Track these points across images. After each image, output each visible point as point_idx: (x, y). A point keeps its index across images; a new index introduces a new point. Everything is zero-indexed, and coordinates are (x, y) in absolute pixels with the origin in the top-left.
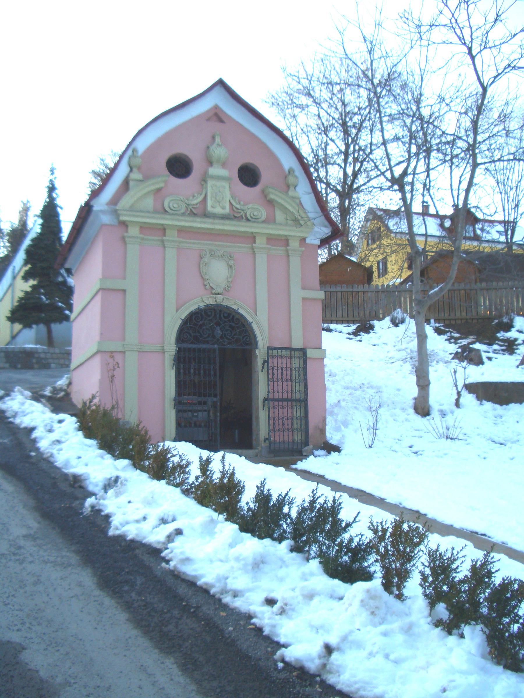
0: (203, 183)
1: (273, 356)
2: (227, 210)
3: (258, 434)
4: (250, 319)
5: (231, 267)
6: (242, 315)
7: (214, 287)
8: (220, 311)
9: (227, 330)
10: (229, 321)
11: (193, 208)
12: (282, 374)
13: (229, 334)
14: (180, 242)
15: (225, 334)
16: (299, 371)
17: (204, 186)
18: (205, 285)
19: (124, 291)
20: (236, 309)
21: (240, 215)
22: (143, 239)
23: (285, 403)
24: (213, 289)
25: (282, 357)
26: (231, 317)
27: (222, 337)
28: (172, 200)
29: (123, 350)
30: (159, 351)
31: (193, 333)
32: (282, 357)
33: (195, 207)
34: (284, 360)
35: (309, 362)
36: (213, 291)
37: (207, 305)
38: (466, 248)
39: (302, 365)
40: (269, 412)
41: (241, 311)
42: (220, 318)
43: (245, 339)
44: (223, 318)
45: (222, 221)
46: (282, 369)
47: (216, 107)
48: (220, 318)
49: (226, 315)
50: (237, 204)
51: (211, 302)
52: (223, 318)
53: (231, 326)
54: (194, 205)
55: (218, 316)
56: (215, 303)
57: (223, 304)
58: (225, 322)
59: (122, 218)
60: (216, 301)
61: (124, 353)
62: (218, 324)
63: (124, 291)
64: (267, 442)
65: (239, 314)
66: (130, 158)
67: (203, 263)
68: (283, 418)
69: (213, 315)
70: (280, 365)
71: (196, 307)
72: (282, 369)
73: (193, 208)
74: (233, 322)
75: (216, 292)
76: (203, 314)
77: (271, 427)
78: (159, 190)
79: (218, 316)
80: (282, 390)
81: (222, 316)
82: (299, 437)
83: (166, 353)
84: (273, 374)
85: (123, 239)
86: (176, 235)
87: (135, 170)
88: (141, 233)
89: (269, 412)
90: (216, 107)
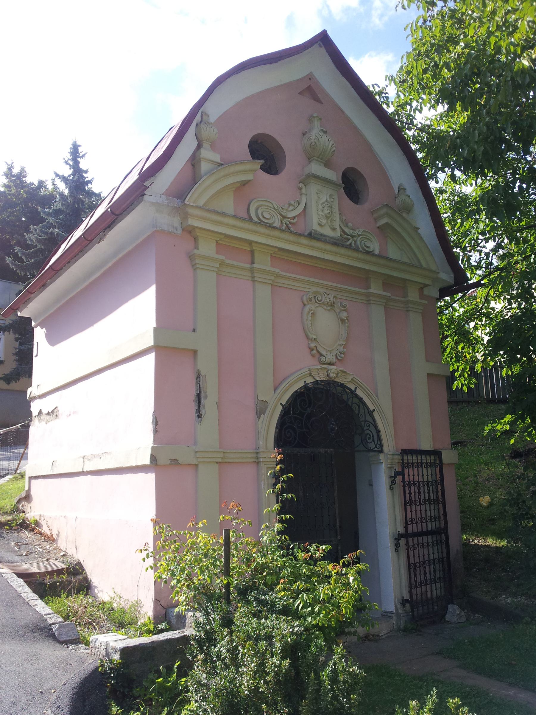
0: (301, 185)
2: (337, 234)
5: (343, 321)
7: (324, 353)
11: (290, 223)
14: (278, 276)
17: (304, 191)
18: (312, 350)
19: (195, 352)
20: (353, 389)
22: (222, 264)
24: (322, 355)
29: (195, 462)
30: (251, 451)
36: (323, 359)
37: (316, 382)
38: (58, 208)
45: (334, 249)
47: (310, 77)
51: (321, 377)
56: (326, 378)
57: (337, 380)
59: (193, 222)
61: (197, 465)
63: (195, 352)
64: (408, 605)
66: (197, 125)
67: (308, 313)
71: (301, 384)
75: (328, 361)
77: (413, 582)
78: (244, 184)
83: (262, 465)
84: (410, 494)
85: (191, 257)
86: (270, 264)
87: (205, 145)
88: (217, 253)
90: (310, 77)
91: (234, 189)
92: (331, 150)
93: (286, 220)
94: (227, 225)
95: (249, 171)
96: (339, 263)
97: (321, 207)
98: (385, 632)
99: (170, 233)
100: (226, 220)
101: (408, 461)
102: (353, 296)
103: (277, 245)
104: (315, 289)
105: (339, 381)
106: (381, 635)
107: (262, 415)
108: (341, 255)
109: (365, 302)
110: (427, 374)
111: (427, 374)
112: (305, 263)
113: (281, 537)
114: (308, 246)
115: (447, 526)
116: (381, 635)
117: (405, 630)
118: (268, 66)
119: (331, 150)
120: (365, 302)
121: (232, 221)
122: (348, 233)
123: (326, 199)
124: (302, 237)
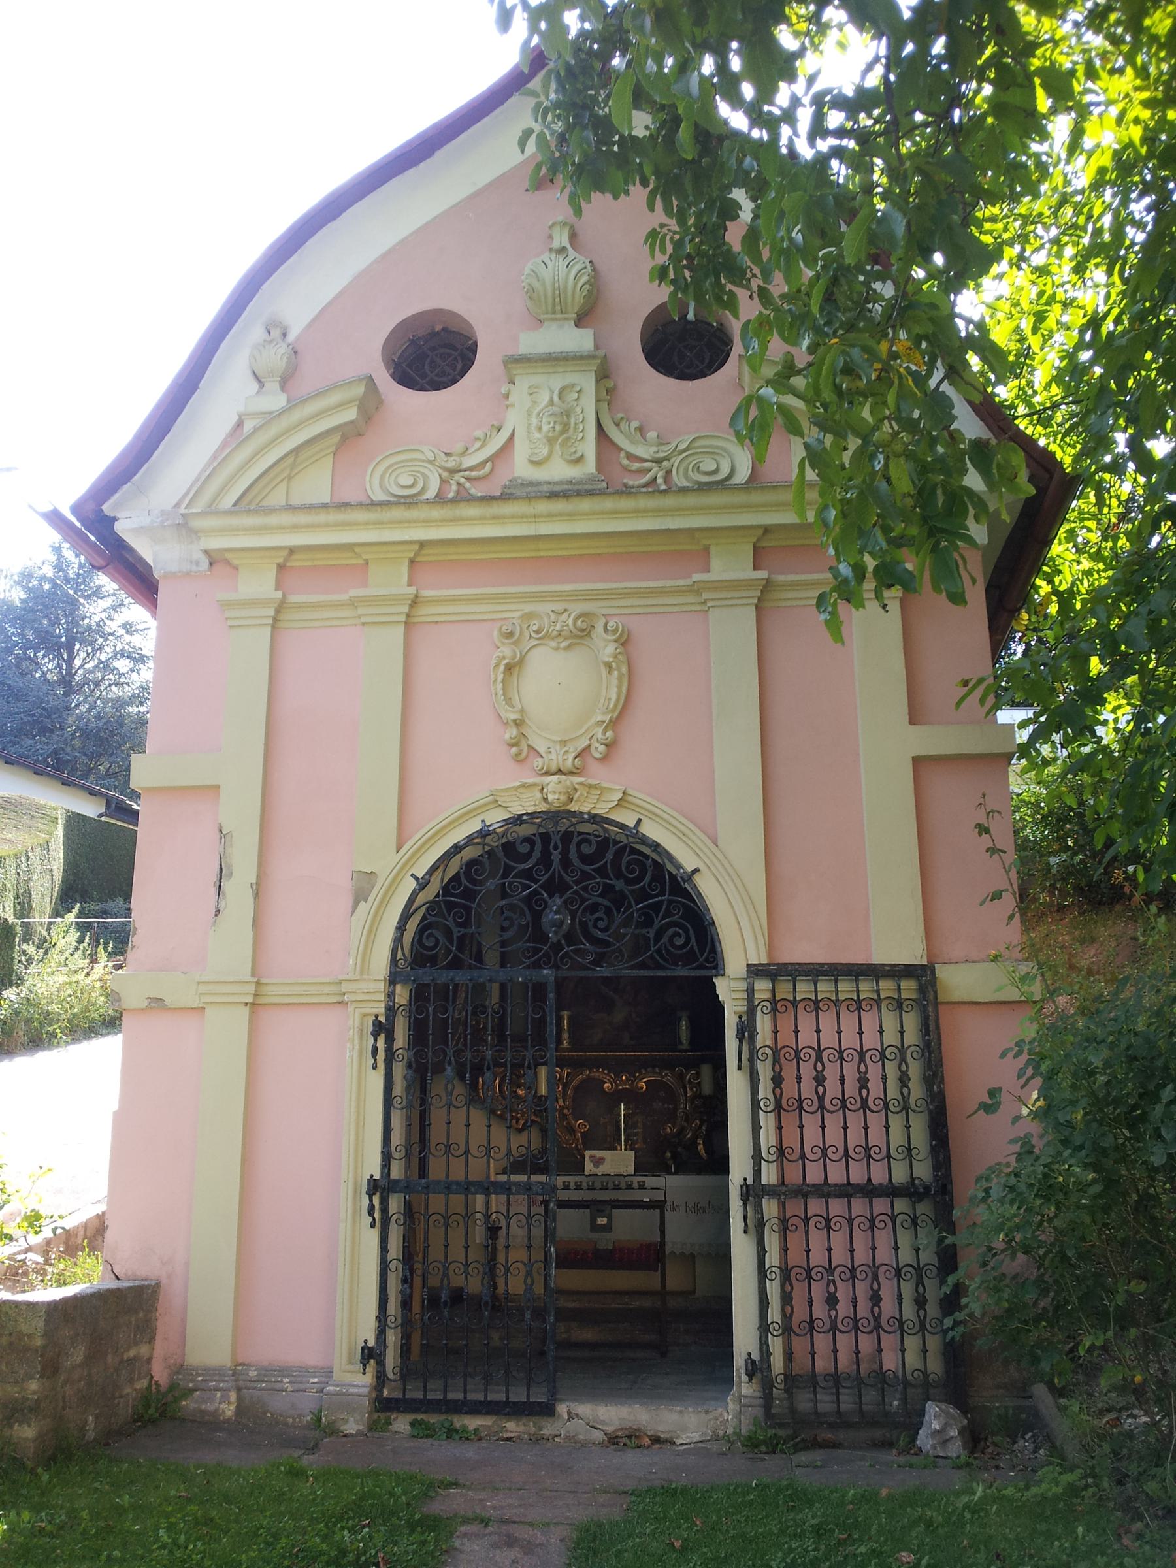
1: (859, 1002)
3: (399, 1202)
4: (688, 861)
6: (656, 846)
8: (567, 837)
9: (594, 908)
10: (602, 872)
11: (468, 479)
12: (820, 1080)
13: (601, 924)
15: (584, 925)
16: (903, 1060)
20: (631, 823)
21: (647, 478)
23: (837, 1207)
25: (858, 1005)
26: (610, 856)
27: (570, 938)
28: (382, 477)
31: (459, 925)
32: (816, 1004)
33: (474, 474)
34: (827, 1021)
35: (946, 1018)
39: (912, 1037)
40: (761, 1243)
41: (650, 830)
42: (566, 863)
43: (665, 940)
44: (576, 862)
46: (819, 1058)
48: (566, 863)
49: (587, 850)
50: (633, 442)
51: (527, 804)
52: (576, 862)
53: (608, 890)
54: (470, 469)
55: (556, 856)
56: (543, 807)
57: (573, 807)
58: (585, 876)
60: (545, 800)
62: (555, 887)
63: (218, 787)
65: (644, 840)
68: (830, 1270)
69: (537, 854)
70: (850, 1040)
72: (819, 1058)
73: (468, 479)
74: (619, 875)
76: (501, 854)
77: (775, 1314)
79: (556, 856)
80: (824, 1151)
81: (573, 854)
82: (912, 1360)
89: (761, 1243)
91: (332, 449)
92: (576, 284)
93: (457, 477)
94: (281, 528)
95: (340, 405)
96: (627, 532)
97: (534, 421)
98: (696, 1437)
99: (188, 574)
100: (273, 520)
101: (858, 996)
102: (650, 602)
103: (407, 538)
104: (577, 608)
105: (585, 809)
106: (678, 1442)
107: (362, 903)
108: (586, 514)
109: (698, 608)
110: (914, 759)
111: (914, 759)
112: (509, 555)
113: (1138, 1191)
114: (594, 513)
115: (948, 1175)
116: (678, 1442)
117: (752, 1444)
118: (411, 172)
119: (576, 284)
120: (698, 608)
121: (287, 519)
122: (646, 456)
123: (547, 399)
124: (462, 505)
